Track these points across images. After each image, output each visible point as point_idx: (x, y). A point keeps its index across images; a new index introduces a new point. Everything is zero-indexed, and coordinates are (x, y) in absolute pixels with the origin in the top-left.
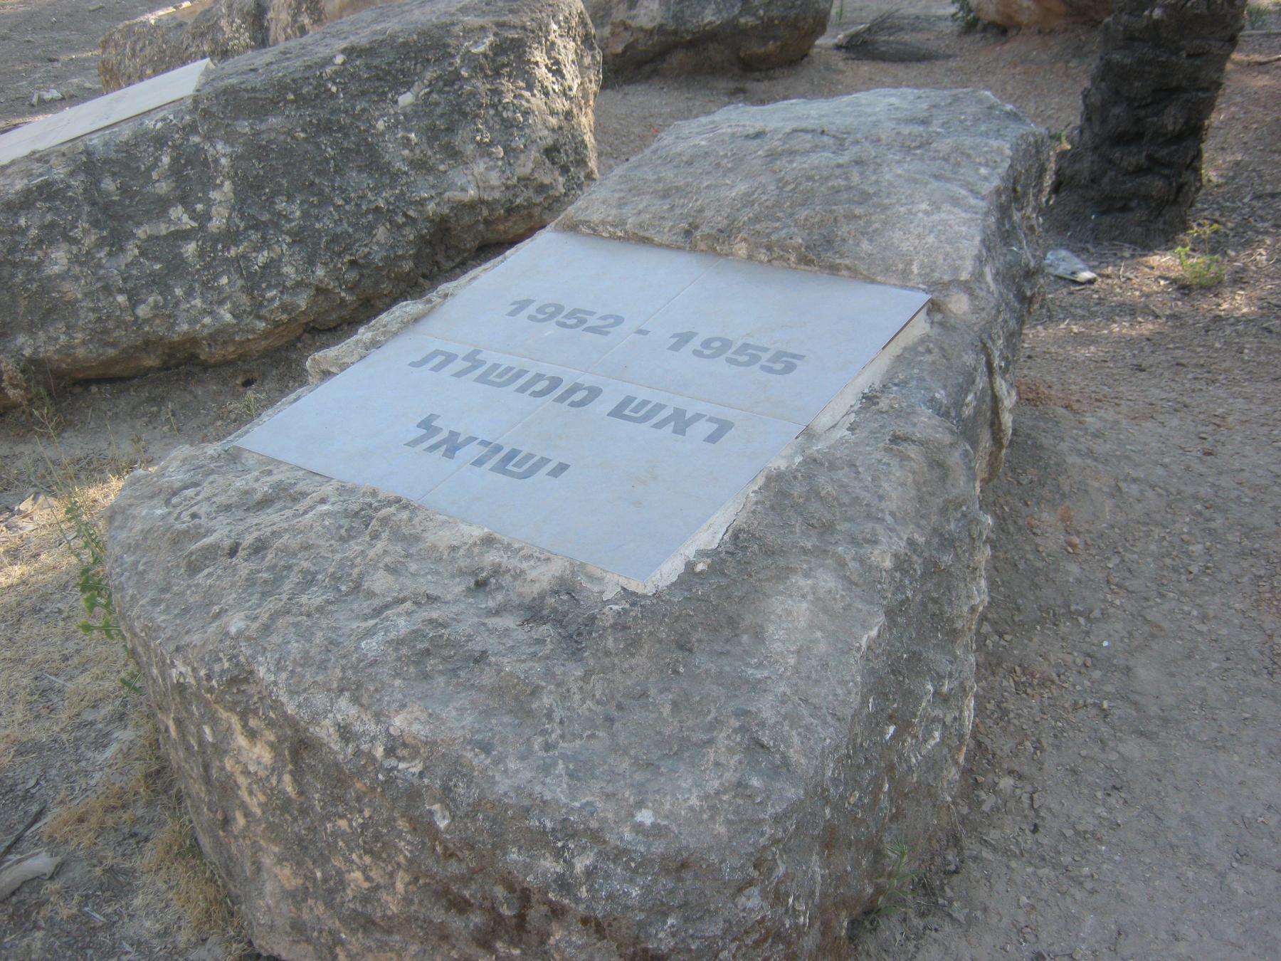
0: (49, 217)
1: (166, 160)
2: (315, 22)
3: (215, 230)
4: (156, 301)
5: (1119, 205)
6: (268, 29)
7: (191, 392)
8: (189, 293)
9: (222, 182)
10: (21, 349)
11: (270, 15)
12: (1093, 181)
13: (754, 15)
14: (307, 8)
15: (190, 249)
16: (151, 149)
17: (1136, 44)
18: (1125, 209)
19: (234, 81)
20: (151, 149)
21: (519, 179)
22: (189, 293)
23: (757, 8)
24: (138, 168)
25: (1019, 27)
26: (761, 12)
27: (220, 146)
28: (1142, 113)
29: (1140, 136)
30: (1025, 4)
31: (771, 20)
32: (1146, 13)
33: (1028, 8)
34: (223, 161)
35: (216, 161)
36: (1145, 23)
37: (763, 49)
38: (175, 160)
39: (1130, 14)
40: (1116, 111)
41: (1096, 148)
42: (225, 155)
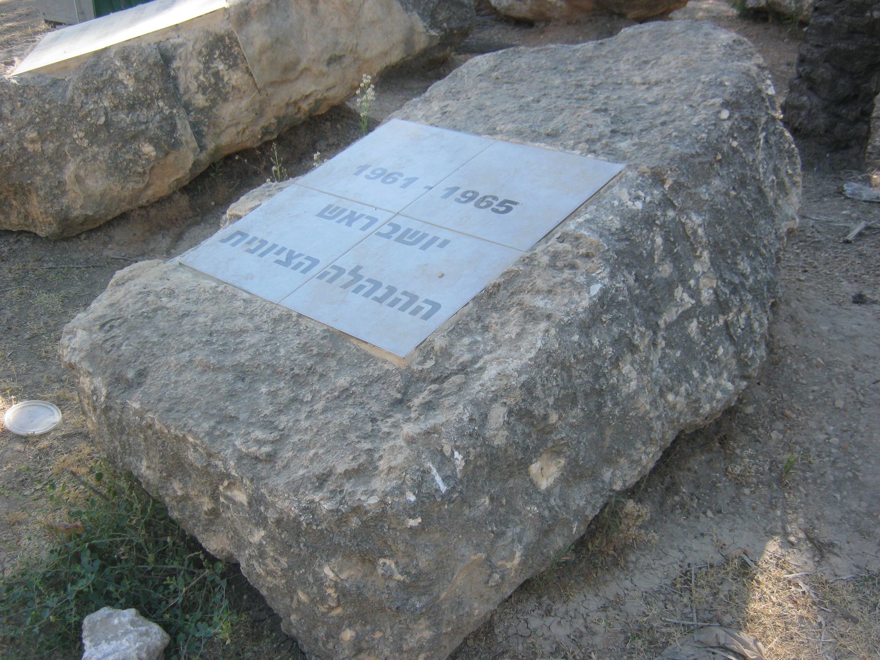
0: (616, 330)
1: (659, 240)
2: (230, 67)
3: (708, 303)
4: (686, 390)
5: (843, 145)
6: (175, 78)
7: (689, 469)
8: (703, 374)
9: (701, 253)
10: (611, 484)
11: (175, 64)
12: (826, 131)
13: (440, 28)
14: (221, 54)
15: (693, 327)
16: (645, 231)
17: (856, 35)
18: (847, 147)
19: (548, 147)
20: (645, 231)
21: (126, 178)
22: (703, 374)
23: (442, 22)
24: (641, 253)
25: (548, 21)
26: (445, 25)
27: (694, 217)
28: (859, 82)
29: (856, 97)
30: (559, 4)
31: (452, 30)
32: (868, 14)
33: (561, 7)
34: (700, 231)
35: (695, 232)
36: (866, 21)
37: (442, 54)
38: (666, 240)
39: (851, 15)
40: (842, 82)
41: (825, 109)
42: (700, 226)
